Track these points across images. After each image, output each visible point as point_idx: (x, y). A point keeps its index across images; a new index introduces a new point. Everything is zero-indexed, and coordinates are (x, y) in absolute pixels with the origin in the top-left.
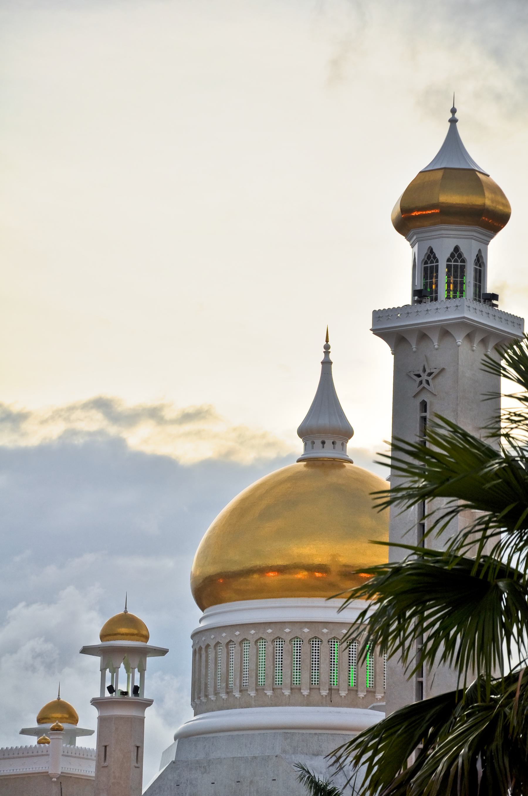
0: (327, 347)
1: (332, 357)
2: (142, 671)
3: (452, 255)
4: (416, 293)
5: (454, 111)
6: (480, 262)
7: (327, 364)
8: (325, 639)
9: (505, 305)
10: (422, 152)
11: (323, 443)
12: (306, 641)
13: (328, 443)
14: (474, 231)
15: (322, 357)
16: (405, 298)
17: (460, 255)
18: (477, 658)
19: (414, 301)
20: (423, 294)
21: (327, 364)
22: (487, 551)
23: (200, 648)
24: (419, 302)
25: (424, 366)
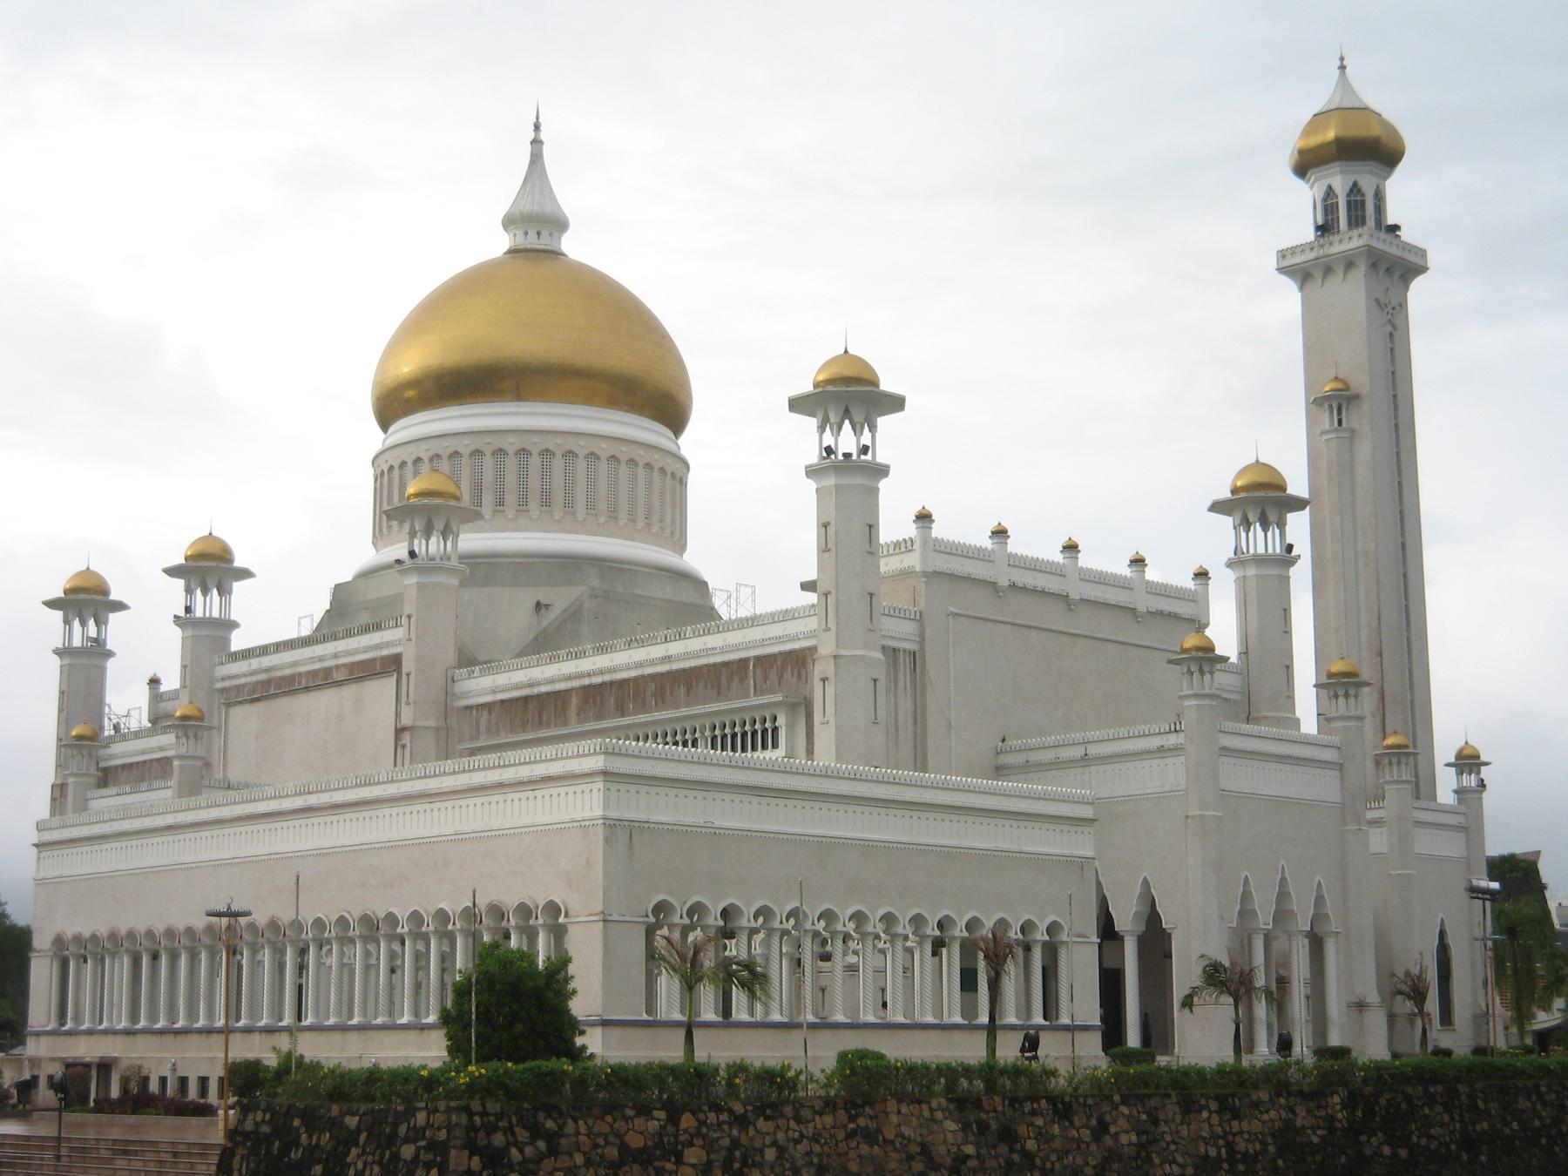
0: (537, 127)
1: (543, 136)
2: (873, 429)
3: (1351, 191)
4: (1318, 228)
5: (1342, 59)
6: (1379, 197)
7: (537, 142)
8: (604, 456)
9: (1405, 235)
10: (1318, 95)
11: (539, 234)
12: (445, 458)
13: (545, 234)
14: (1371, 165)
15: (532, 135)
16: (1309, 235)
17: (1359, 191)
18: (272, 993)
19: (1317, 237)
20: (1324, 229)
21: (537, 142)
22: (1009, 1050)
23: (382, 473)
24: (1322, 236)
25: (1283, 880)
